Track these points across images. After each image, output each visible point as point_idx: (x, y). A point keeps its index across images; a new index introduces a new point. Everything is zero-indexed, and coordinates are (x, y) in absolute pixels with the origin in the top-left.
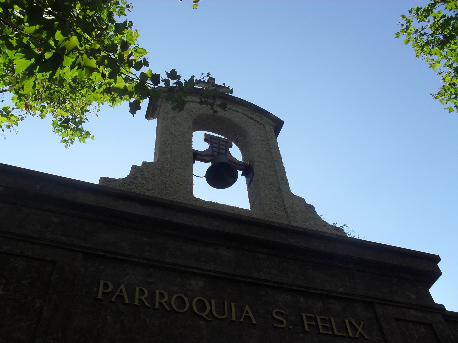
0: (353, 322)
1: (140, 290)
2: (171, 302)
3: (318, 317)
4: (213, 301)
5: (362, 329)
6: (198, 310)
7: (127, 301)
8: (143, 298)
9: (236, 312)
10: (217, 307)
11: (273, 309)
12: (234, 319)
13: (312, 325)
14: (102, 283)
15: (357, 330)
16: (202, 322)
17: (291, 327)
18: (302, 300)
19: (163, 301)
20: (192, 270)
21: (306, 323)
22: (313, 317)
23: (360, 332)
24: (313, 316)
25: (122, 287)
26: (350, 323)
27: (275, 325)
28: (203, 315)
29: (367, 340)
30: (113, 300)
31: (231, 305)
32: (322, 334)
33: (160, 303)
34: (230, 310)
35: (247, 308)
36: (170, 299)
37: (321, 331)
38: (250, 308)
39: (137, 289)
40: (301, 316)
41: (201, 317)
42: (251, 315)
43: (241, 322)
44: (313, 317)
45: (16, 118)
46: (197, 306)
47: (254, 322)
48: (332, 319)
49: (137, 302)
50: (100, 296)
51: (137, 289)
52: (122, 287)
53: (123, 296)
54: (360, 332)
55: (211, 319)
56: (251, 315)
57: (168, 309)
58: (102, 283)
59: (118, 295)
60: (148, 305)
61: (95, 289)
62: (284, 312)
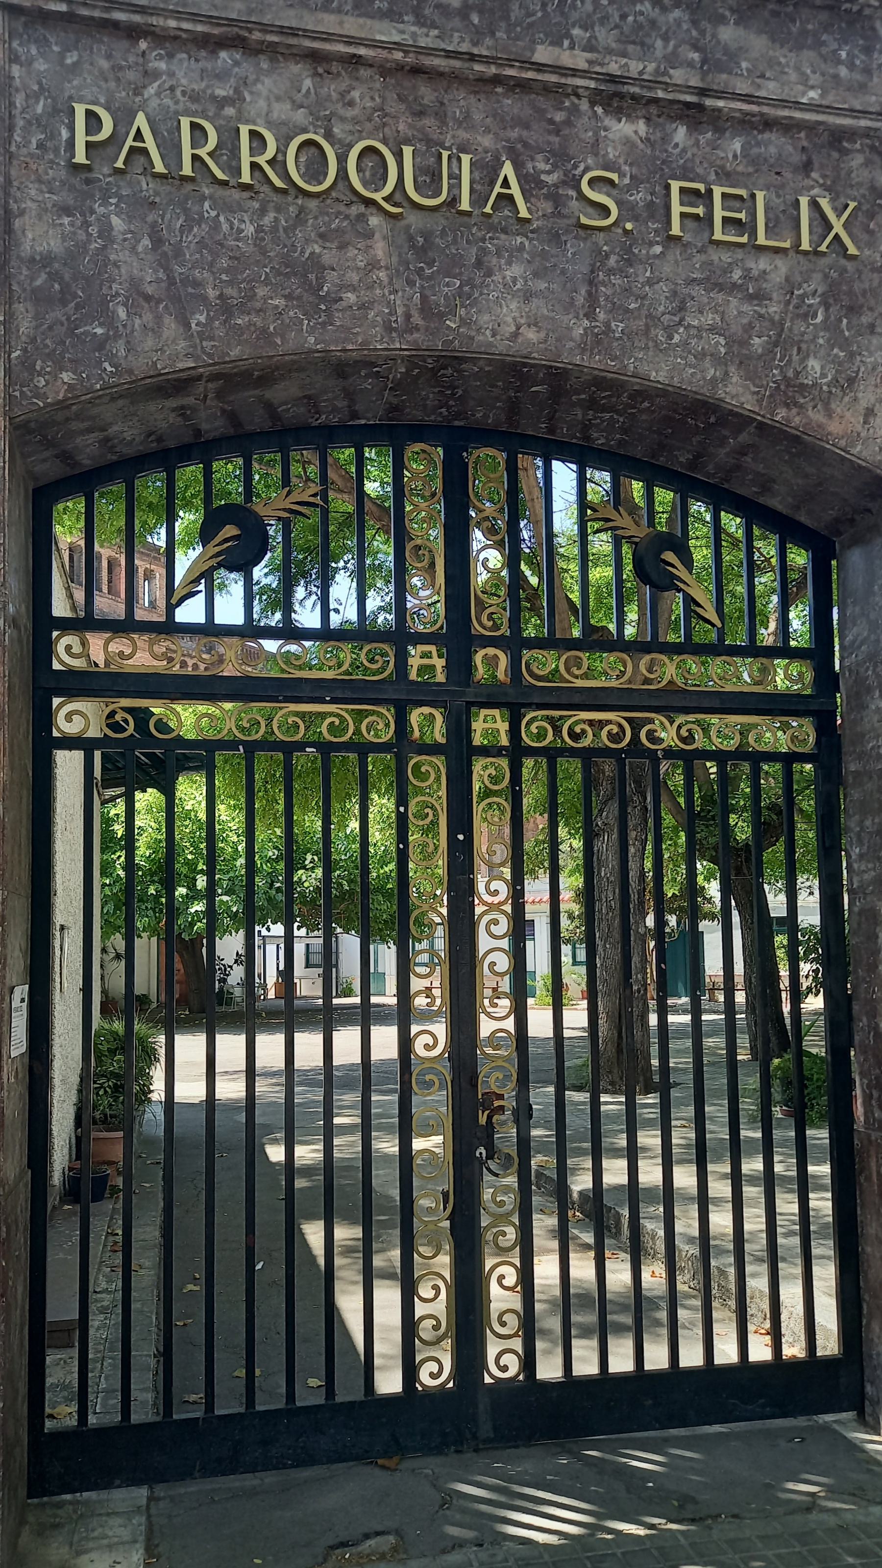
0: (825, 204)
1: (194, 126)
2: (285, 162)
3: (717, 191)
4: (407, 151)
5: (845, 226)
6: (365, 184)
7: (159, 167)
8: (203, 152)
9: (472, 182)
10: (418, 170)
11: (587, 169)
12: (465, 205)
13: (696, 217)
14: (80, 111)
15: (830, 227)
16: (374, 221)
17: (629, 226)
18: (680, 134)
19: (261, 160)
20: (308, 43)
21: (676, 209)
22: (703, 191)
23: (837, 235)
24: (702, 187)
25: (141, 121)
26: (814, 204)
27: (584, 220)
28: (378, 197)
29: (853, 258)
30: (120, 164)
31: (459, 160)
32: (718, 243)
33: (255, 167)
34: (456, 177)
35: (508, 170)
36: (282, 150)
37: (718, 235)
38: (518, 167)
39: (185, 123)
40: (668, 187)
41: (369, 203)
42: (515, 190)
43: (488, 216)
44: (703, 191)
45: (164, 263)
46: (359, 169)
47: (524, 213)
48: (760, 196)
49: (187, 170)
50: (80, 157)
51: (185, 123)
52: (141, 121)
53: (145, 152)
54: (837, 235)
55: (400, 210)
56: (515, 190)
57: (278, 183)
58: (80, 111)
59: (131, 147)
60: (220, 175)
61: (65, 134)
62: (614, 177)
